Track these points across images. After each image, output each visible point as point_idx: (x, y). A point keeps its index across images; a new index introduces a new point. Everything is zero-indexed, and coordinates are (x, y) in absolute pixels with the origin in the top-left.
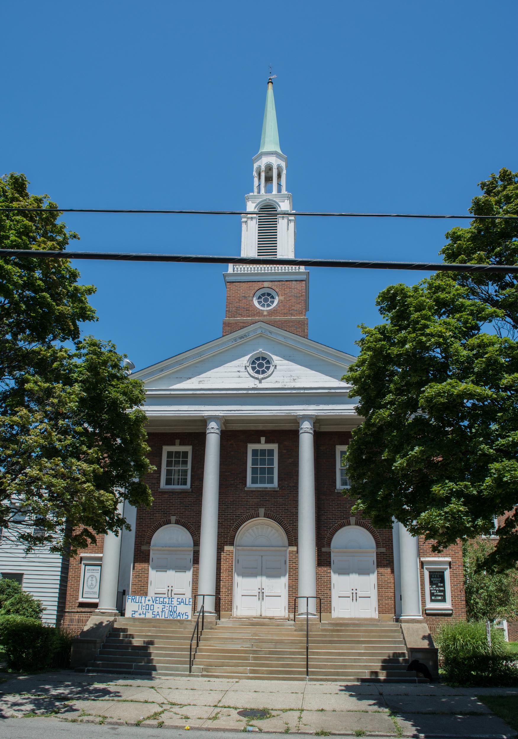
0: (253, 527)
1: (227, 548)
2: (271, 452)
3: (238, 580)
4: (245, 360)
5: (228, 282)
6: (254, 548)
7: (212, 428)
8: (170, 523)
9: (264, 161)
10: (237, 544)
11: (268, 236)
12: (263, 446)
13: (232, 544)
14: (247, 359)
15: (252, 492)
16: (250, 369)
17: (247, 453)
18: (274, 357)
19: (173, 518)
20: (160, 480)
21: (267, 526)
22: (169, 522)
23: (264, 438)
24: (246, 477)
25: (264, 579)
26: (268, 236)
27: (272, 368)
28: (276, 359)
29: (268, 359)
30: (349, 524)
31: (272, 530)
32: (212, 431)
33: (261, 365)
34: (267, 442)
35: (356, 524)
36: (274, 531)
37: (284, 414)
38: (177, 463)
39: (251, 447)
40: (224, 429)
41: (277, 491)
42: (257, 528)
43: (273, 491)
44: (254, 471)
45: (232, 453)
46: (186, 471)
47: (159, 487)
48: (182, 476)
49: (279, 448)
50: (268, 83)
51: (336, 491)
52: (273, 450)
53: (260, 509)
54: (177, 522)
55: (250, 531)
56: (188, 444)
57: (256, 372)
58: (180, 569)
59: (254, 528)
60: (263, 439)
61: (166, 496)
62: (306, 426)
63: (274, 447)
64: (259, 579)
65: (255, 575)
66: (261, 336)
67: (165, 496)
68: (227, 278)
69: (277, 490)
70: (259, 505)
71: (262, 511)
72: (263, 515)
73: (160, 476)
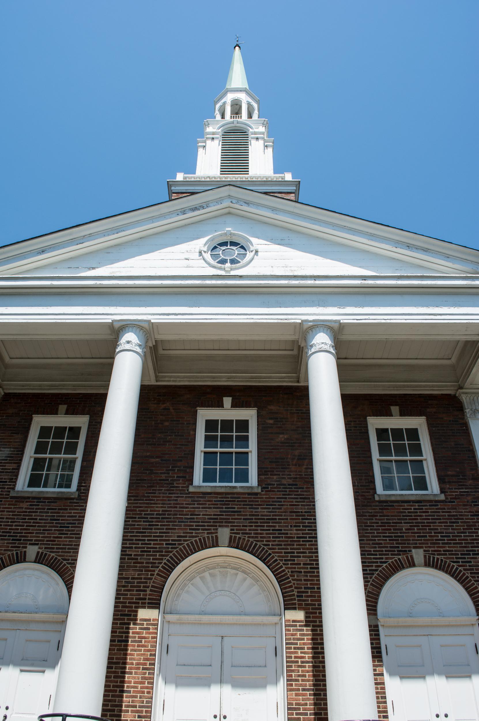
0: (204, 571)
1: (143, 614)
2: (243, 425)
3: (164, 693)
4: (200, 243)
5: (174, 193)
6: (205, 618)
7: (128, 342)
8: (24, 561)
9: (230, 97)
10: (168, 609)
11: (235, 154)
12: (227, 412)
13: (155, 604)
14: (204, 242)
15: (203, 495)
16: (208, 256)
17: (195, 424)
18: (254, 240)
19: (32, 551)
20: (17, 476)
21: (234, 571)
22: (21, 559)
23: (230, 399)
24: (192, 467)
25: (227, 690)
26: (235, 154)
27: (249, 255)
28: (256, 243)
29: (242, 243)
30: (412, 564)
31: (245, 579)
32: (128, 346)
33: (228, 247)
34: (235, 405)
35: (427, 564)
36: (249, 581)
37: (276, 321)
38: (56, 449)
39: (204, 414)
40: (153, 382)
41: (256, 494)
42: (212, 575)
43: (249, 494)
44: (209, 458)
45: (167, 424)
46: (73, 462)
47: (13, 489)
48: (63, 470)
49: (259, 416)
50: (235, 47)
51: (377, 498)
52: (247, 421)
53: (220, 530)
54: (39, 559)
55: (197, 580)
56: (83, 413)
57: (218, 262)
58: (32, 665)
59: (207, 574)
60: (227, 401)
61: (25, 505)
62: (322, 340)
63: (250, 414)
64: (215, 689)
65: (205, 682)
66: (229, 213)
67: (21, 505)
68: (173, 188)
69: (256, 491)
70: (218, 522)
71: (224, 533)
72: (227, 542)
73: (18, 468)
